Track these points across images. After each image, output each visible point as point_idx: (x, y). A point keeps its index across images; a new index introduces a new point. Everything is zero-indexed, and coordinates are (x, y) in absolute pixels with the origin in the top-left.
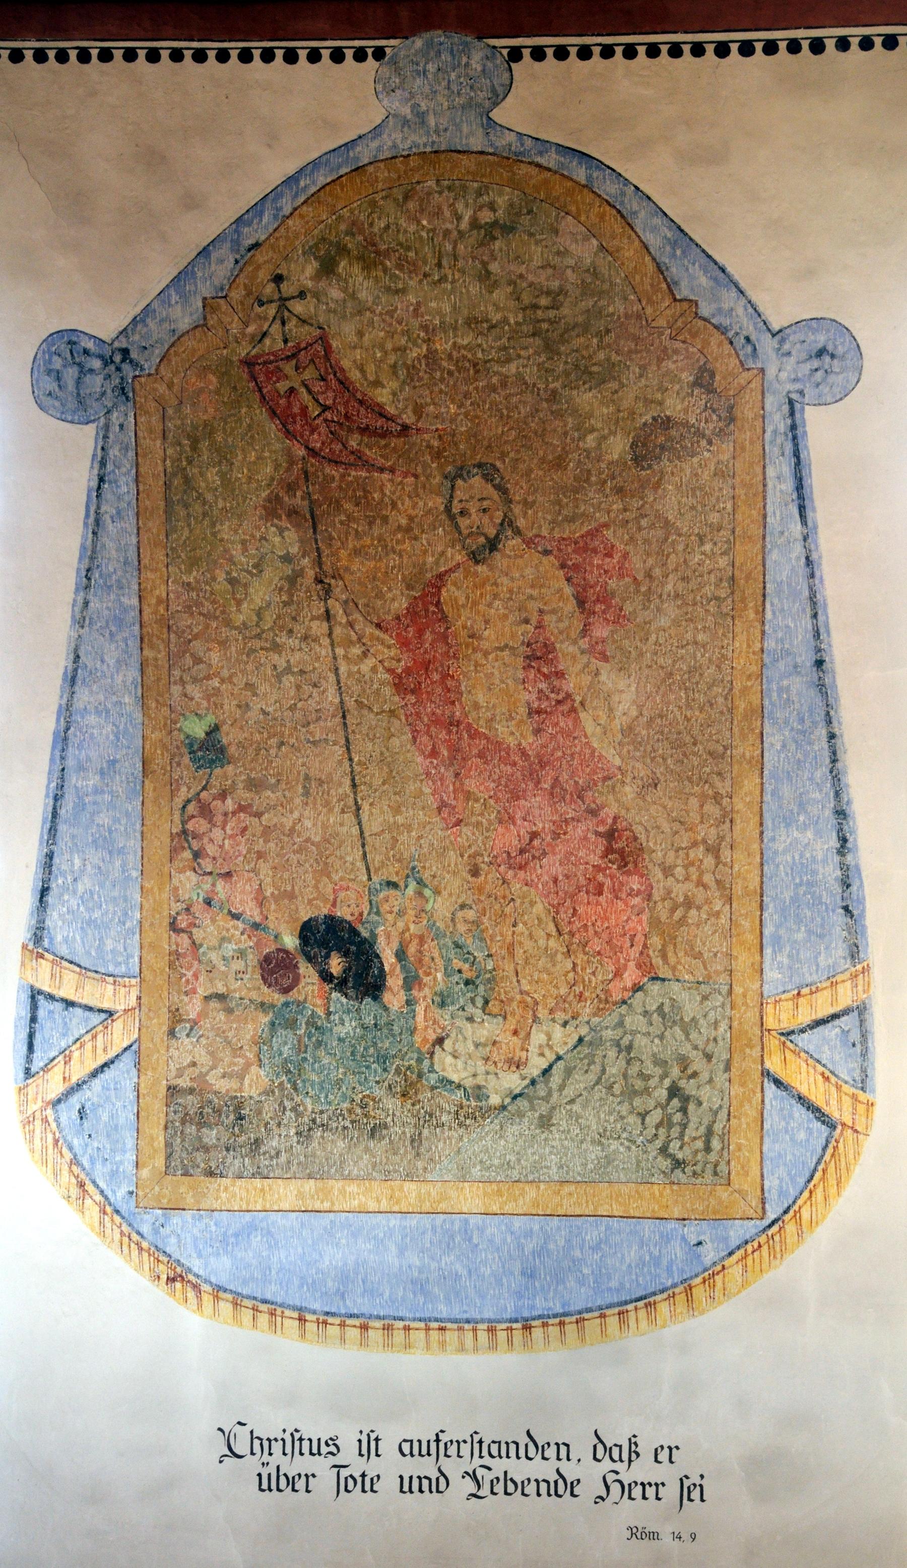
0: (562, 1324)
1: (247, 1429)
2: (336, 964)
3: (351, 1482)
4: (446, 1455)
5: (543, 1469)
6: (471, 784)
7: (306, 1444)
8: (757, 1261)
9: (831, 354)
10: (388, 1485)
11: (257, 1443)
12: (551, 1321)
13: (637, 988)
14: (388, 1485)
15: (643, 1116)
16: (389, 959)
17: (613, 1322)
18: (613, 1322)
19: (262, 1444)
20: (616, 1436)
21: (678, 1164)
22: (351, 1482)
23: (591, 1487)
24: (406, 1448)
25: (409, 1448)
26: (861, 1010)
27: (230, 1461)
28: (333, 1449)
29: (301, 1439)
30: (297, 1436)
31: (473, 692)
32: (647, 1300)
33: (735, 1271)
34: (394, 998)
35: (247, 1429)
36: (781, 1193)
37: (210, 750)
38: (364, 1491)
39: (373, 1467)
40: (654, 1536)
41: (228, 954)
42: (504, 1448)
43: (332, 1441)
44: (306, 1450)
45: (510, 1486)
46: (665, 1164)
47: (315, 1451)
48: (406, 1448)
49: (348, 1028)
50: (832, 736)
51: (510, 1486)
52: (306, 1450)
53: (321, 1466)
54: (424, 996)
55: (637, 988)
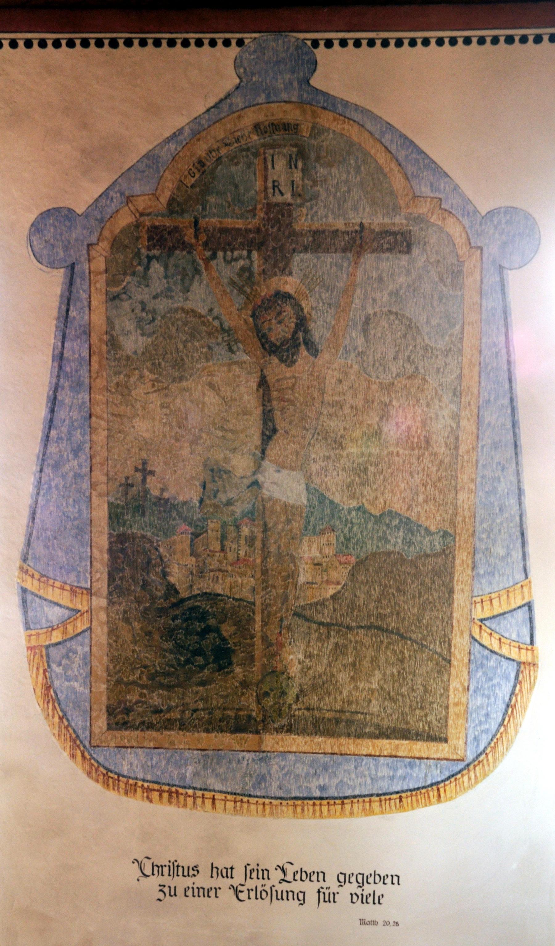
0: (343, 804)
1: (151, 861)
3: (264, 894)
4: (251, 878)
7: (180, 869)
9: (516, 224)
11: (215, 870)
12: (337, 801)
19: (158, 868)
20: (221, 864)
22: (264, 894)
24: (342, 878)
26: (529, 606)
27: (143, 879)
28: (196, 873)
29: (178, 866)
30: (176, 864)
31: (210, 473)
35: (151, 861)
36: (84, 729)
38: (362, 902)
44: (180, 873)
47: (186, 874)
48: (342, 878)
52: (180, 873)
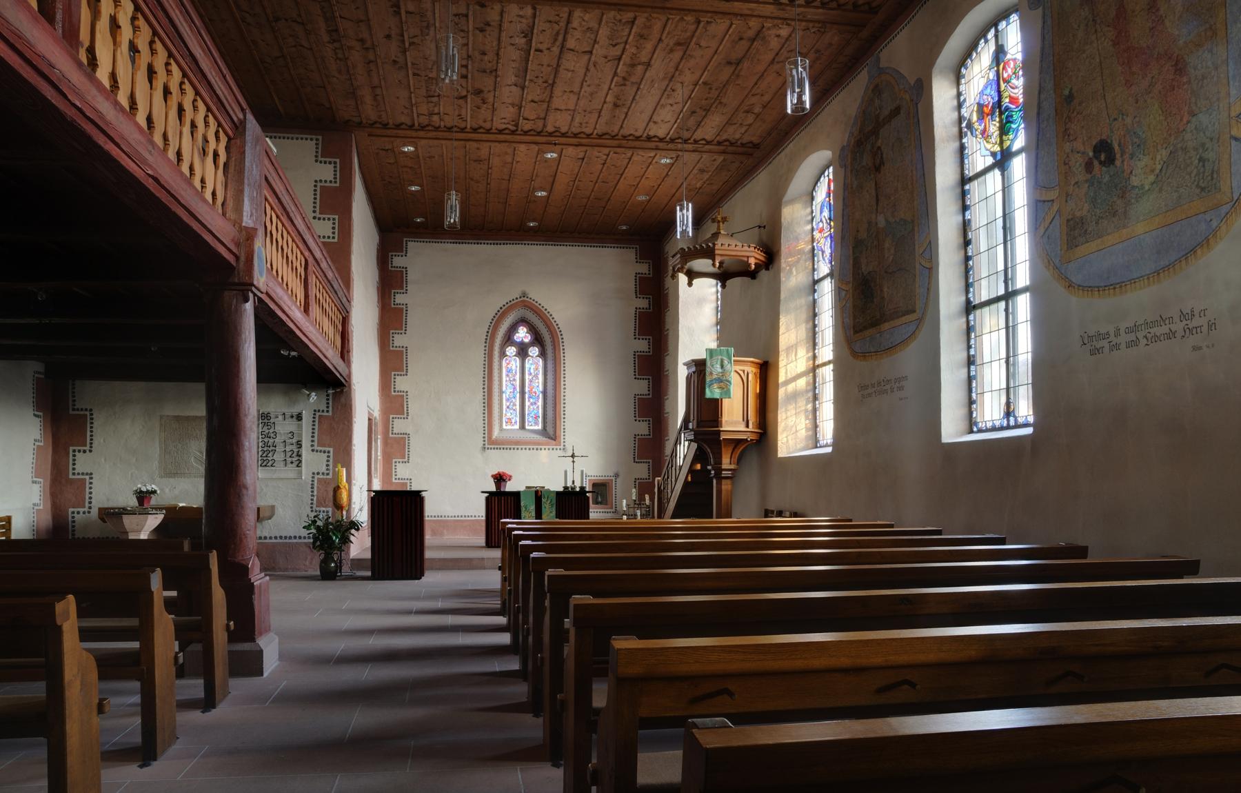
2: (1103, 157)
5: (1164, 329)
6: (1134, 69)
8: (982, 267)
10: (1123, 346)
13: (1188, 122)
14: (1123, 346)
15: (1190, 174)
16: (1116, 147)
17: (1184, 262)
18: (1184, 262)
21: (1203, 189)
23: (1180, 333)
25: (1129, 330)
32: (1193, 251)
33: (1224, 228)
34: (1118, 163)
37: (1070, 98)
39: (1119, 340)
40: (1200, 348)
41: (1077, 162)
42: (1154, 323)
43: (1108, 333)
45: (1156, 338)
46: (1198, 191)
49: (1106, 179)
50: (970, 361)
51: (1156, 338)
53: (1105, 343)
54: (1127, 156)
55: (1188, 122)
